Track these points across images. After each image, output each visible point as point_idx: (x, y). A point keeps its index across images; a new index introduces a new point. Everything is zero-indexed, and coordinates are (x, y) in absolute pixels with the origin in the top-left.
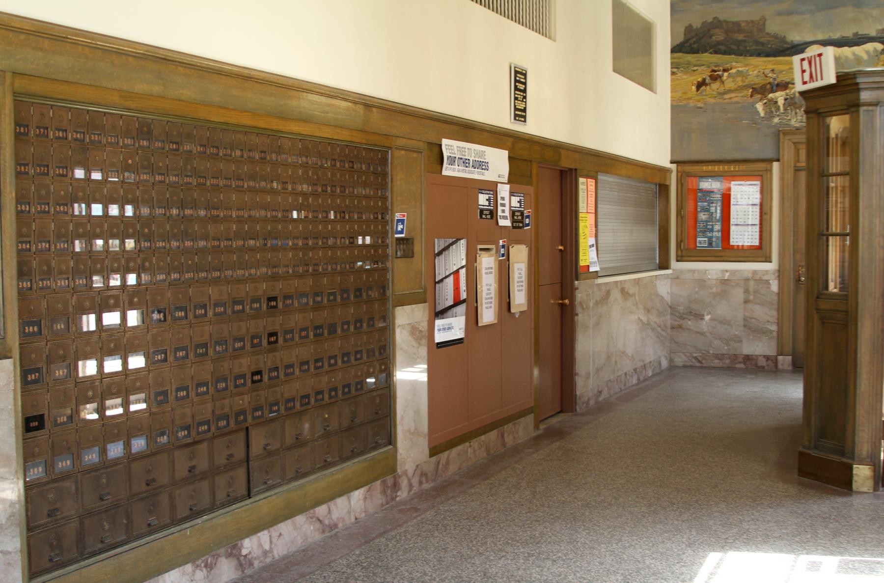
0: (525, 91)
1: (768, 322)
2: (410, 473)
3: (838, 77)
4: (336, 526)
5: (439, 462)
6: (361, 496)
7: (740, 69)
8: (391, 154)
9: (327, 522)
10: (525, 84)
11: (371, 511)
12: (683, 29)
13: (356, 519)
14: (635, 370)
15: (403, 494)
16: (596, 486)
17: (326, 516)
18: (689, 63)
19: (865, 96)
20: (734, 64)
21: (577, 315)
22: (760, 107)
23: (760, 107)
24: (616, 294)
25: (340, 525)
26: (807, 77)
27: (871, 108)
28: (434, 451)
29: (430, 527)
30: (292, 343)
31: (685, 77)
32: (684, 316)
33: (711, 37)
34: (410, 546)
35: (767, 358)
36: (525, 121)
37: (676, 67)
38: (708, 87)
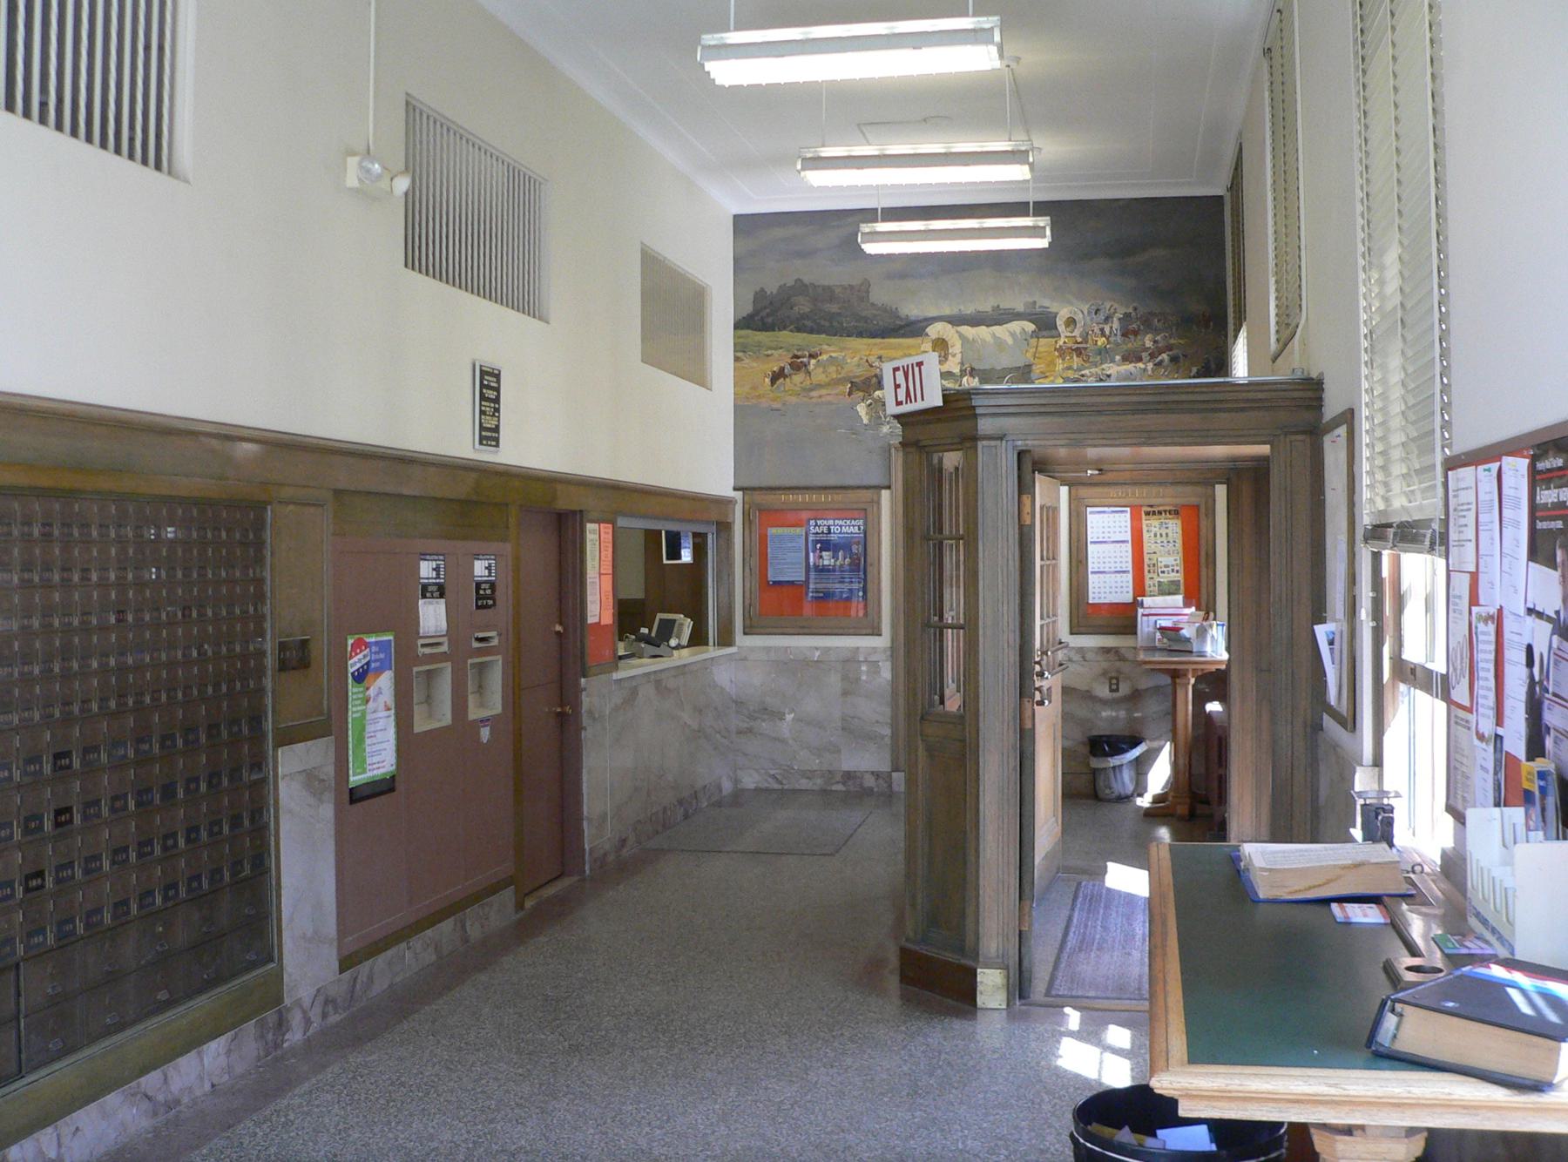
0: (497, 400)
1: (877, 722)
2: (307, 1003)
3: (946, 397)
4: (178, 1102)
5: (355, 980)
6: (220, 1050)
7: (833, 355)
8: (272, 512)
9: (161, 1098)
10: (498, 390)
11: (239, 1070)
12: (751, 297)
13: (213, 1086)
14: (680, 802)
15: (295, 1037)
16: (596, 1011)
17: (160, 1089)
18: (759, 345)
19: (985, 425)
20: (825, 347)
21: (585, 729)
22: (862, 409)
23: (862, 409)
24: (647, 691)
25: (185, 1100)
26: (902, 396)
27: (993, 443)
28: (346, 963)
29: (329, 1097)
30: (96, 821)
31: (755, 364)
32: (756, 715)
33: (792, 308)
34: (292, 1134)
35: (877, 775)
36: (497, 445)
37: (741, 349)
38: (788, 380)
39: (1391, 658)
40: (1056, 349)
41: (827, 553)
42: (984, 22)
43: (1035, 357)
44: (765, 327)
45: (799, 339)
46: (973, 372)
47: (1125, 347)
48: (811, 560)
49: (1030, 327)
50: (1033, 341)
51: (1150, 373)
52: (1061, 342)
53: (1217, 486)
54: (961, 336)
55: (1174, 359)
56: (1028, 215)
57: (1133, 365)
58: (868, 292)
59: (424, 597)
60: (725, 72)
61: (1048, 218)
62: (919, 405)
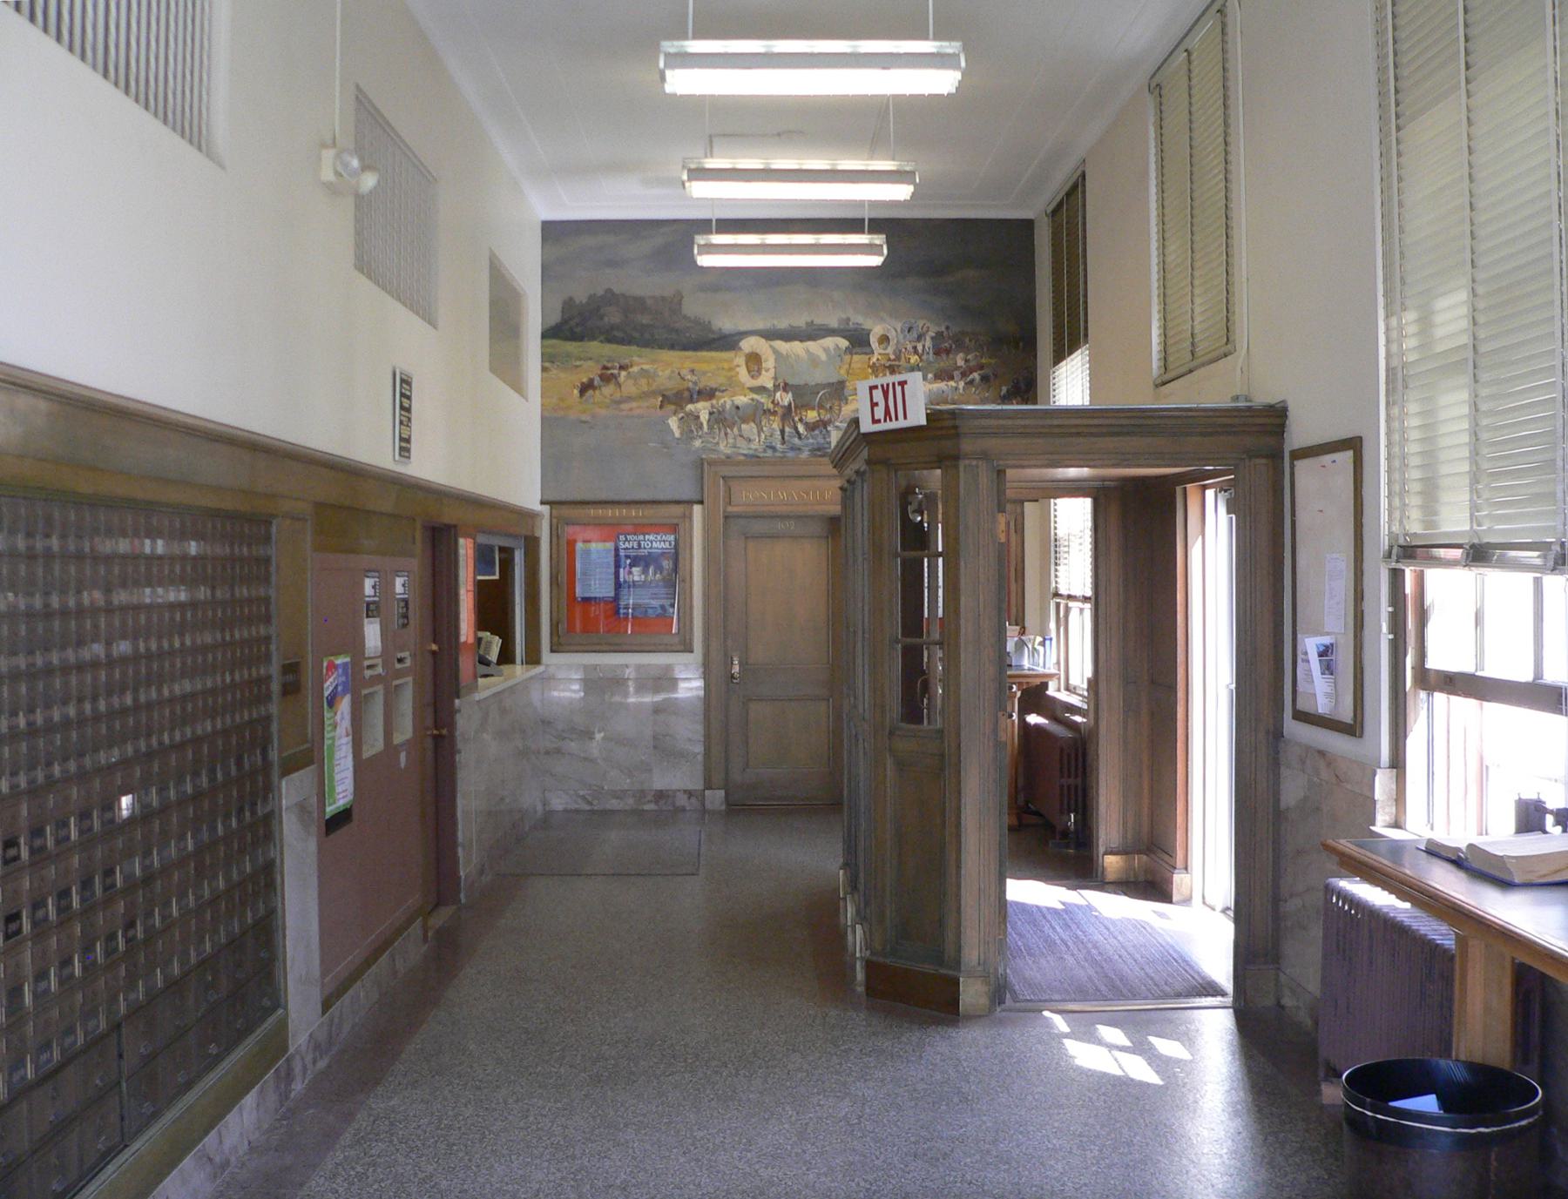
7: (645, 367)
13: (250, 1143)
15: (298, 1087)
18: (569, 355)
19: (967, 445)
20: (636, 359)
21: (459, 752)
22: (673, 423)
23: (673, 423)
26: (880, 412)
31: (562, 375)
32: (565, 735)
37: (548, 359)
38: (597, 392)
39: (1413, 668)
40: (869, 366)
41: (638, 569)
42: (947, 47)
43: (848, 373)
44: (574, 337)
45: (608, 349)
46: (786, 387)
47: (937, 366)
48: (621, 575)
49: (844, 343)
50: (847, 358)
51: (961, 391)
52: (874, 360)
53: (1026, 504)
54: (775, 351)
55: (984, 379)
56: (863, 232)
57: (945, 383)
58: (680, 303)
59: (368, 616)
60: (681, 82)
61: (884, 236)
62: (901, 423)
